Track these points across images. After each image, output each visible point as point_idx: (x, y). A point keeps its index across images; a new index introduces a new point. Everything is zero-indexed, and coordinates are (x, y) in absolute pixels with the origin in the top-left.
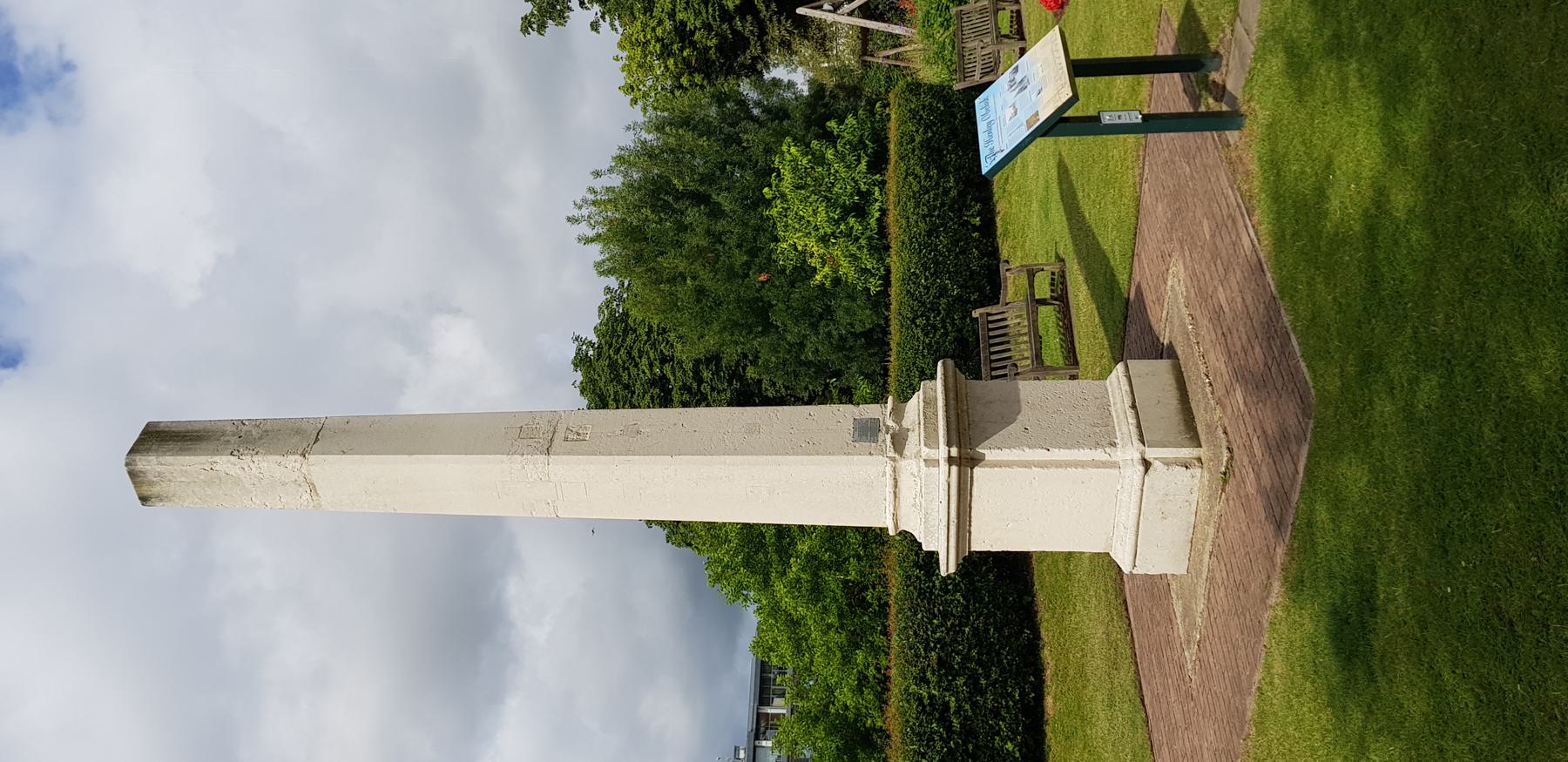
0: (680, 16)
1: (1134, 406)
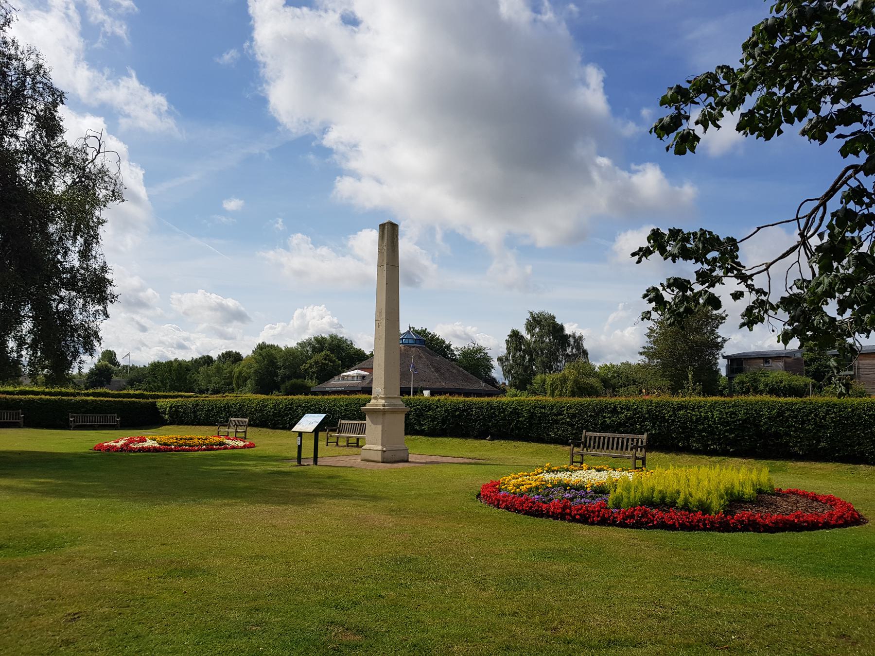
1: (370, 450)
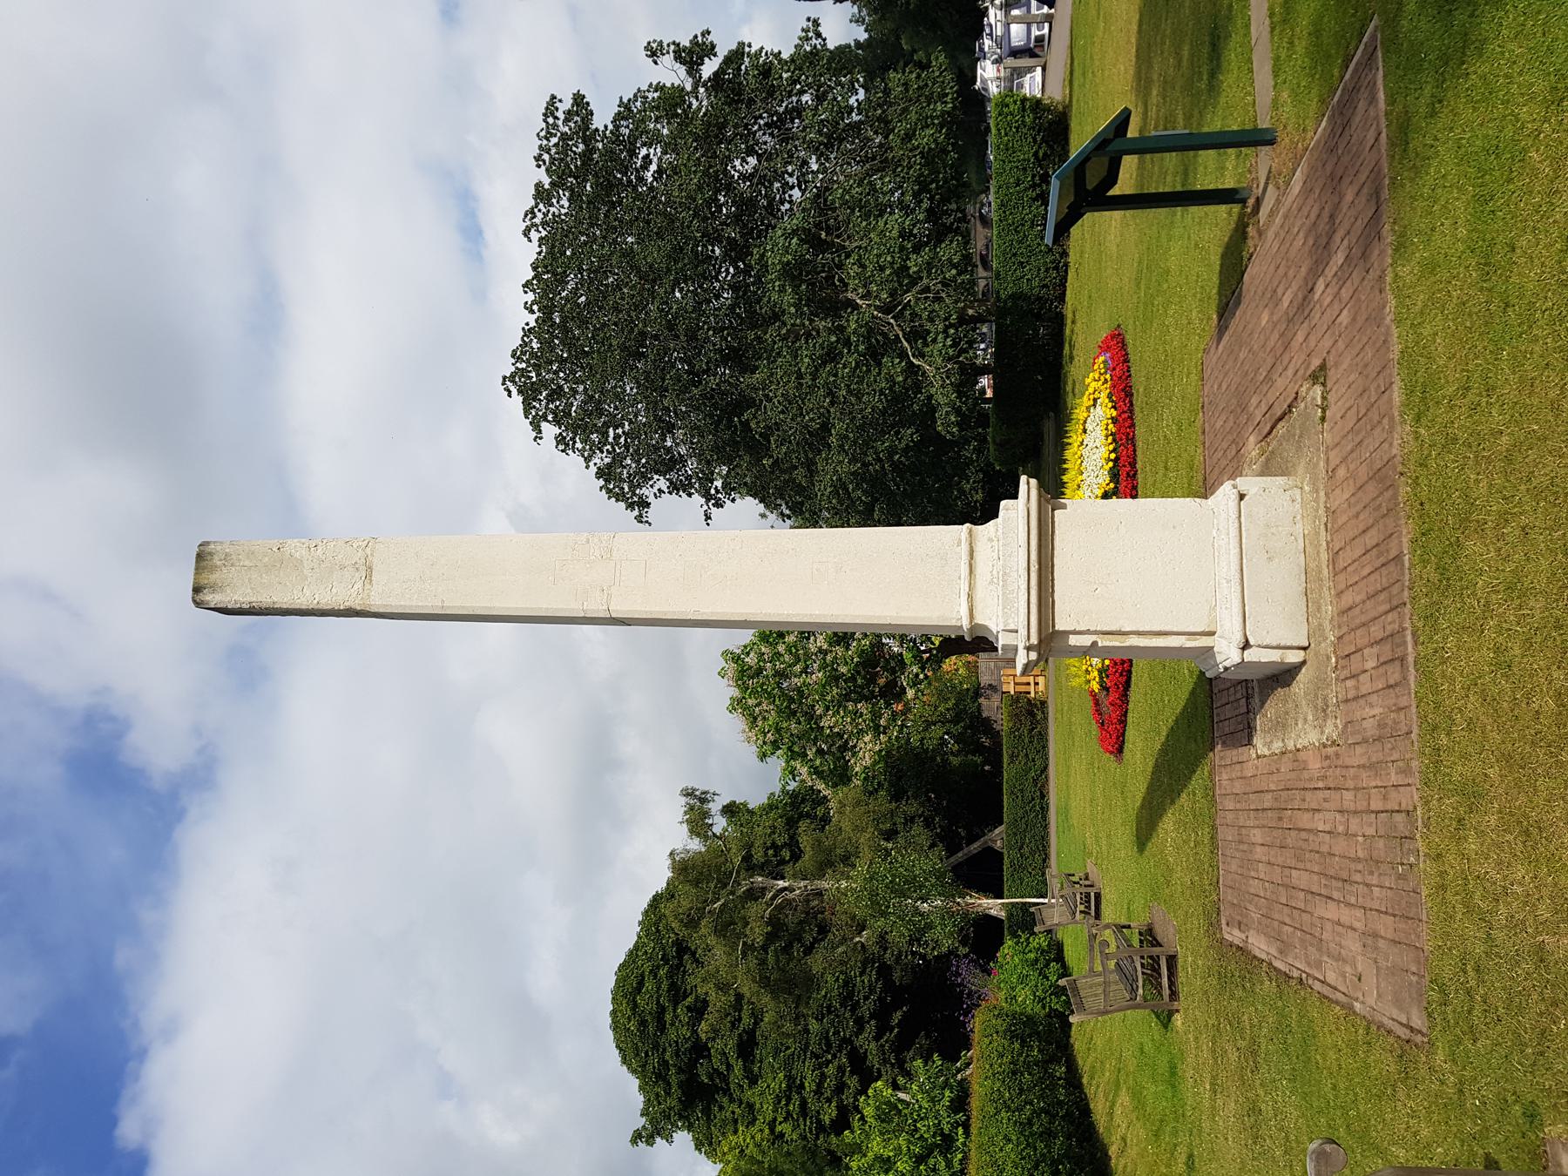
0: (779, 1128)
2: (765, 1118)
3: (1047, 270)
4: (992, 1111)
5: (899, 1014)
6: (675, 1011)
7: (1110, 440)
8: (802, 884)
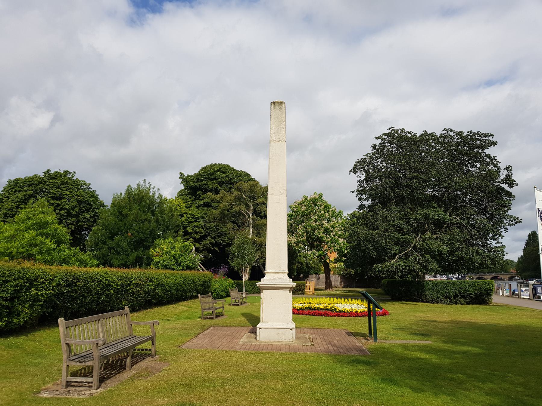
0: (185, 215)
2: (188, 211)
3: (431, 297)
4: (183, 276)
5: (217, 249)
6: (216, 183)
7: (351, 311)
8: (251, 221)
